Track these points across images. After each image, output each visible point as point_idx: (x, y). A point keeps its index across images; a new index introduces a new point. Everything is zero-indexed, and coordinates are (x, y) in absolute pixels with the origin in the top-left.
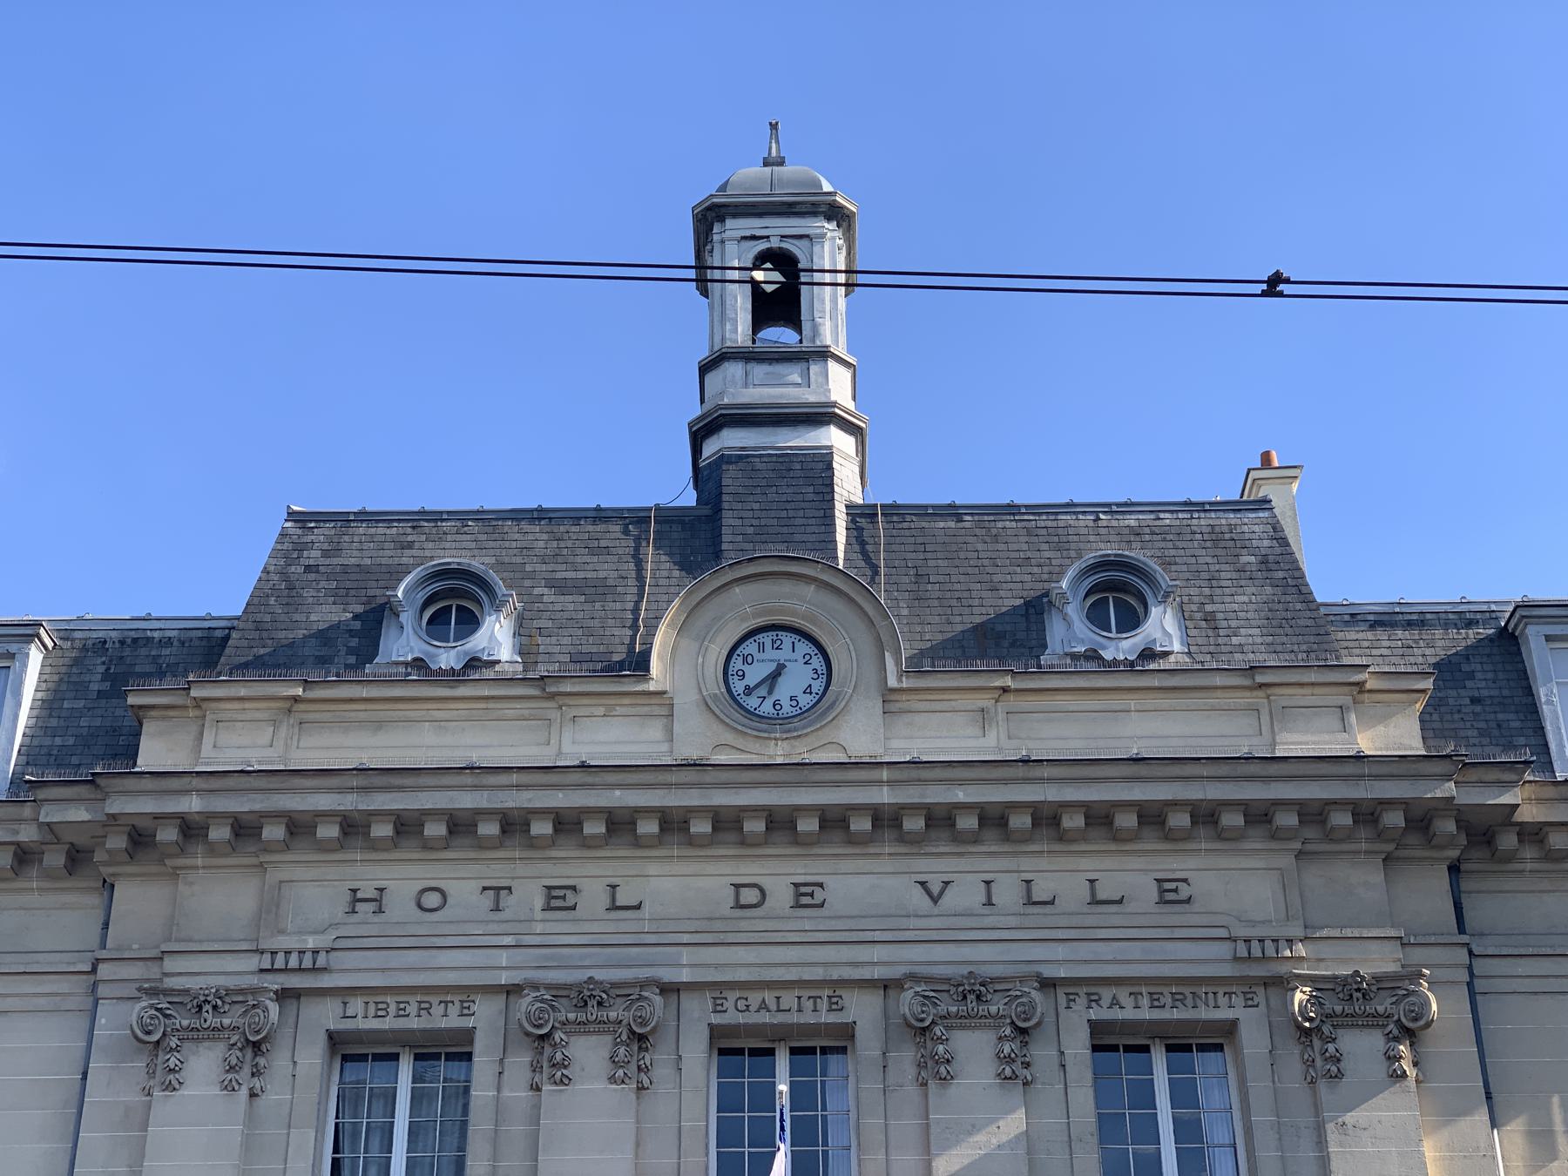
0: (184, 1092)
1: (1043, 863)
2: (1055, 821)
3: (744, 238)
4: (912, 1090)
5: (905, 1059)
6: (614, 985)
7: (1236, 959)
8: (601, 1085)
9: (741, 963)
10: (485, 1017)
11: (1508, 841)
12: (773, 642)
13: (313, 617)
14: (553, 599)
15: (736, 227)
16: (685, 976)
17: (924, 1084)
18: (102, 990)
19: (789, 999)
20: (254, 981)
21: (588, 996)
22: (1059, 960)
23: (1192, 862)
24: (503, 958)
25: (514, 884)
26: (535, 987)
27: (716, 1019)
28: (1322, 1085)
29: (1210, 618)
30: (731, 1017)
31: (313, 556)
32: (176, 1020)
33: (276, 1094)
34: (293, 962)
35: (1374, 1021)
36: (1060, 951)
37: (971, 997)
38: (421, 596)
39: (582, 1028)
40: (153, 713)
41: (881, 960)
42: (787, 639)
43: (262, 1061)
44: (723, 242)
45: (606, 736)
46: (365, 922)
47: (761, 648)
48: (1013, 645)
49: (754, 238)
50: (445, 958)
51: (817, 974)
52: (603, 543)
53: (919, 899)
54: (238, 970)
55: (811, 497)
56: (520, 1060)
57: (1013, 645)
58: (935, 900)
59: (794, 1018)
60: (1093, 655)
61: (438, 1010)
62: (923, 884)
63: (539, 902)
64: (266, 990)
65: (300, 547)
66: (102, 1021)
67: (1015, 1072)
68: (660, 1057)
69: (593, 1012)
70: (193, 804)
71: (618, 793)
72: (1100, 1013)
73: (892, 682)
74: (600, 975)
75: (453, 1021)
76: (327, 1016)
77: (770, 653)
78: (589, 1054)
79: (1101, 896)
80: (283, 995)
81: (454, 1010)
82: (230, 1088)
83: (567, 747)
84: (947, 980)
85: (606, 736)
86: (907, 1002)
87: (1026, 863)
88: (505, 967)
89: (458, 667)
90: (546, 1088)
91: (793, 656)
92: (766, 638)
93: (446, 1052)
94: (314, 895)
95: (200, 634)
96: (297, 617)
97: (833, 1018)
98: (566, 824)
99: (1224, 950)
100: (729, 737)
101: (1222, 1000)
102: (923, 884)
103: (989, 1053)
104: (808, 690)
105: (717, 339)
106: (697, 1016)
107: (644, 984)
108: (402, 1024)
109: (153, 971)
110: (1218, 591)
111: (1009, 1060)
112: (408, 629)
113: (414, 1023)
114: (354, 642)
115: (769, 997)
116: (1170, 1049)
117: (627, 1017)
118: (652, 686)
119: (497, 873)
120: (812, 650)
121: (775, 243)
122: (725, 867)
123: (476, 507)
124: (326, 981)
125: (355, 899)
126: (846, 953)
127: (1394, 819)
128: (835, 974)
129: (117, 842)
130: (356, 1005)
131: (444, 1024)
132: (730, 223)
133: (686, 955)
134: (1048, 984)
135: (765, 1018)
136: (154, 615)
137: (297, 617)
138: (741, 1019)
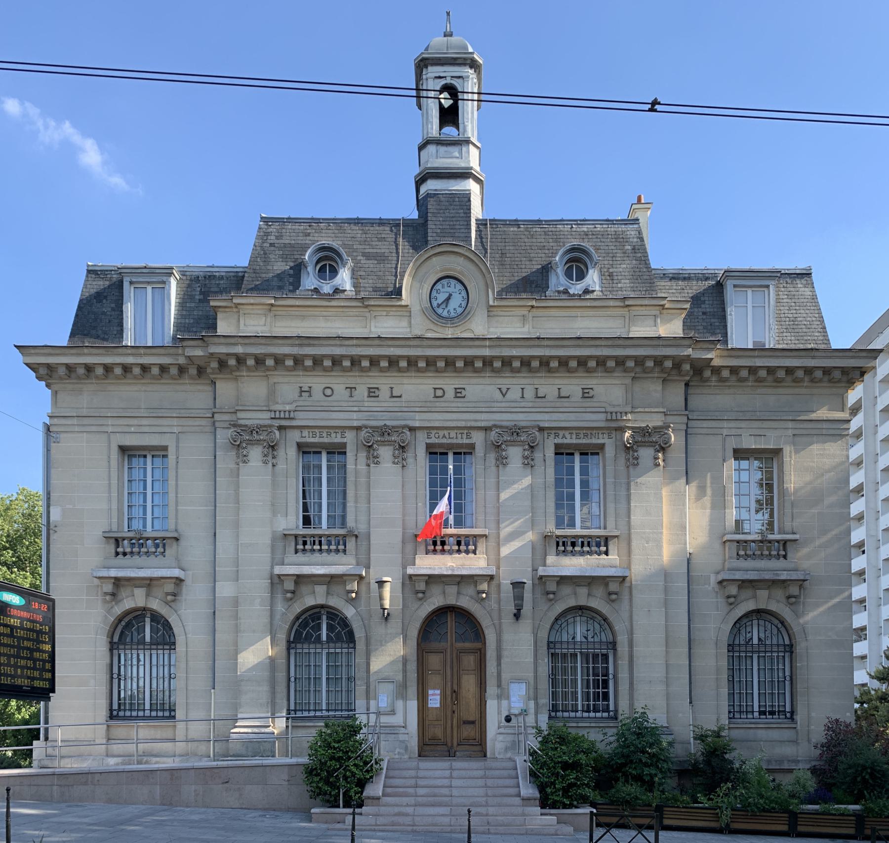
1: (542, 381)
3: (436, 77)
4: (494, 469)
5: (492, 457)
6: (393, 427)
7: (607, 420)
8: (390, 465)
9: (436, 419)
11: (707, 373)
16: (417, 424)
18: (217, 424)
21: (384, 431)
22: (546, 420)
25: (357, 386)
27: (428, 441)
29: (611, 275)
30: (434, 440)
32: (244, 438)
33: (281, 466)
35: (652, 444)
38: (315, 259)
39: (383, 443)
41: (485, 420)
42: (453, 282)
43: (275, 453)
46: (305, 401)
47: (443, 287)
48: (536, 286)
49: (440, 77)
51: (463, 424)
52: (383, 236)
53: (498, 396)
54: (262, 418)
55: (462, 215)
56: (363, 455)
57: (536, 286)
60: (566, 292)
61: (333, 435)
63: (366, 394)
65: (267, 234)
66: (218, 436)
68: (409, 455)
69: (387, 438)
72: (559, 441)
73: (491, 303)
76: (295, 436)
78: (385, 453)
79: (562, 395)
80: (280, 428)
81: (339, 435)
82: (265, 462)
83: (373, 329)
86: (493, 435)
87: (536, 381)
92: (445, 282)
93: (337, 451)
99: (602, 416)
100: (432, 326)
103: (520, 455)
104: (460, 306)
106: (422, 440)
107: (404, 427)
108: (321, 440)
109: (234, 417)
111: (526, 458)
113: (326, 440)
115: (446, 432)
117: (398, 439)
118: (403, 303)
120: (462, 287)
121: (448, 81)
122: (430, 381)
123: (333, 217)
124: (294, 423)
127: (668, 364)
129: (214, 365)
130: (305, 433)
131: (336, 441)
132: (430, 68)
134: (541, 429)
135: (444, 441)
136: (216, 265)
138: (437, 441)
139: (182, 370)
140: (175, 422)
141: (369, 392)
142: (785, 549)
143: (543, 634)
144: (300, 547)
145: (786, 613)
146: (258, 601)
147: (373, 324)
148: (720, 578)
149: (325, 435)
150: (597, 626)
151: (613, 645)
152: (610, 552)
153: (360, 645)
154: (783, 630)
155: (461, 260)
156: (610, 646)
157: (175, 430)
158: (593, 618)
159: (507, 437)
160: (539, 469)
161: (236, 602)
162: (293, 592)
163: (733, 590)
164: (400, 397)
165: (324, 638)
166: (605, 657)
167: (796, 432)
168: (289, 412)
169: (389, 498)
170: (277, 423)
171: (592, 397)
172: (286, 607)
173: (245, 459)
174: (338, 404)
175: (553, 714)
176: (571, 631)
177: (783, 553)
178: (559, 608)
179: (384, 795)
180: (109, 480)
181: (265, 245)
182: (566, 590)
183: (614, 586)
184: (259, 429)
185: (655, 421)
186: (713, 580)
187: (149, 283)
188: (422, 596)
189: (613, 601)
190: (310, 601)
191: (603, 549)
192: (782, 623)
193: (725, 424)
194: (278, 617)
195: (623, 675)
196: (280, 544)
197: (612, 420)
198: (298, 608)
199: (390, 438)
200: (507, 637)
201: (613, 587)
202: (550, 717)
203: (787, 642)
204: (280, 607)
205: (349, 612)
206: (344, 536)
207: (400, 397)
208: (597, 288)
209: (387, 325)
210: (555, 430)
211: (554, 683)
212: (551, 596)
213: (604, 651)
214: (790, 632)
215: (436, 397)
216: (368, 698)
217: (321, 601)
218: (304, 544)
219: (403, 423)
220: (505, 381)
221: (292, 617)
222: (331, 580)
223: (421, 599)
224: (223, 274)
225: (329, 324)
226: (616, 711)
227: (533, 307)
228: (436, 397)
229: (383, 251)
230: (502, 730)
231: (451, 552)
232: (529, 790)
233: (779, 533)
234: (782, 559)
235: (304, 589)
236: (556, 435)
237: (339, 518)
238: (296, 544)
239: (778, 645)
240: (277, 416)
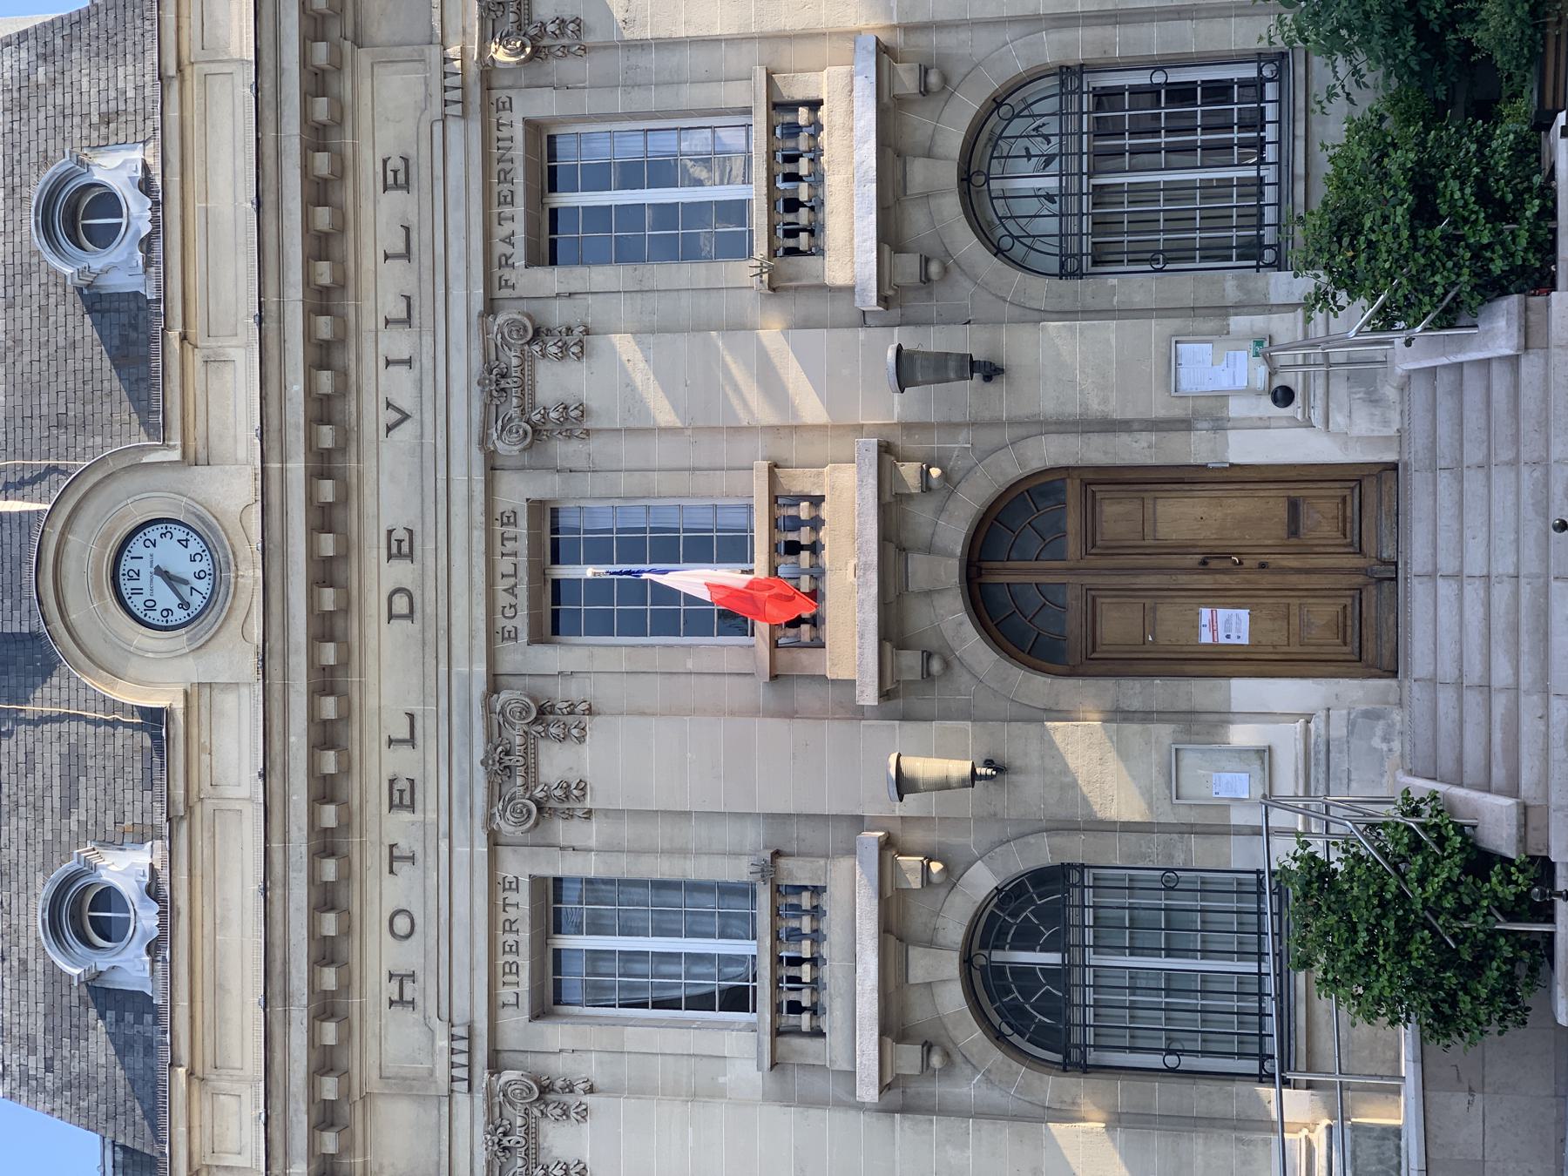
2: (324, 292)
4: (594, 444)
5: (564, 450)
6: (489, 739)
7: (464, 115)
8: (586, 750)
9: (468, 614)
12: (131, 579)
14: (82, 810)
16: (481, 669)
19: (505, 565)
20: (479, 1097)
21: (500, 766)
22: (466, 295)
24: (461, 850)
25: (387, 842)
26: (490, 818)
27: (524, 637)
28: (588, 424)
30: (522, 623)
31: (35, 1064)
33: (590, 1068)
34: (462, 1059)
36: (458, 292)
37: (503, 383)
38: (80, 949)
39: (531, 770)
42: (127, 564)
43: (559, 1083)
45: (232, 751)
46: (424, 991)
47: (137, 591)
48: (135, 328)
50: (461, 909)
51: (479, 536)
52: (22, 758)
53: (406, 432)
54: (469, 1113)
56: (563, 831)
58: (405, 417)
59: (523, 560)
60: (146, 244)
61: (512, 913)
62: (389, 429)
63: (405, 816)
64: (489, 1084)
67: (576, 342)
69: (516, 760)
70: (297, 467)
71: (292, 739)
72: (519, 256)
73: (176, 455)
74: (479, 754)
75: (523, 898)
76: (516, 1024)
77: (143, 582)
80: (495, 1066)
81: (512, 897)
82: (584, 1114)
84: (486, 406)
85: (232, 751)
86: (508, 448)
87: (368, 323)
88: (471, 848)
90: (588, 804)
91: (147, 559)
92: (127, 586)
94: (395, 1042)
96: (102, 1078)
98: (325, 790)
99: (455, 128)
101: (505, 132)
102: (389, 429)
104: (184, 543)
106: (520, 656)
108: (525, 949)
110: (77, 108)
111: (564, 348)
112: (115, 961)
113: (525, 936)
114: (129, 1017)
115: (501, 585)
116: (553, 188)
117: (520, 726)
118: (179, 705)
119: (375, 859)
124: (482, 1026)
125: (400, 1001)
126: (459, 508)
128: (479, 518)
130: (507, 994)
131: (525, 906)
133: (460, 668)
135: (523, 590)
137: (102, 1078)
138: (523, 612)
143: (1040, 290)
146: (951, 1153)
147: (230, 792)
149: (510, 938)
150: (1017, 127)
151: (1069, 75)
152: (811, 94)
153: (1075, 849)
156: (1073, 84)
158: (995, 140)
159: (514, 412)
160: (594, 310)
162: (928, 1047)
165: (1054, 958)
166: (1104, 97)
172: (968, 1070)
173: (574, 791)
174: (434, 898)
175: (1269, 256)
176: (1032, 206)
178: (966, 243)
179: (1513, 791)
182: (917, 222)
183: (907, 83)
184: (498, 1130)
189: (945, 80)
190: (953, 998)
191: (803, 115)
194: (995, 1097)
196: (799, 1080)
198: (971, 1035)
200: (1048, 404)
201: (907, 80)
202: (1279, 265)
204: (968, 1089)
205: (982, 881)
206: (777, 890)
208: (137, 155)
210: (492, 264)
211: (1176, 255)
212: (934, 268)
213: (1087, 102)
215: (410, 615)
216: (1226, 831)
217: (951, 966)
218: (797, 1012)
221: (996, 1056)
222: (895, 932)
223: (947, 665)
225: (235, 915)
226: (1260, 58)
227: (184, 338)
228: (410, 615)
229: (56, 759)
230: (1317, 416)
232: (1498, 332)
234: (823, 112)
235: (919, 1014)
237: (723, 904)
238: (797, 1032)
240: (463, 1045)
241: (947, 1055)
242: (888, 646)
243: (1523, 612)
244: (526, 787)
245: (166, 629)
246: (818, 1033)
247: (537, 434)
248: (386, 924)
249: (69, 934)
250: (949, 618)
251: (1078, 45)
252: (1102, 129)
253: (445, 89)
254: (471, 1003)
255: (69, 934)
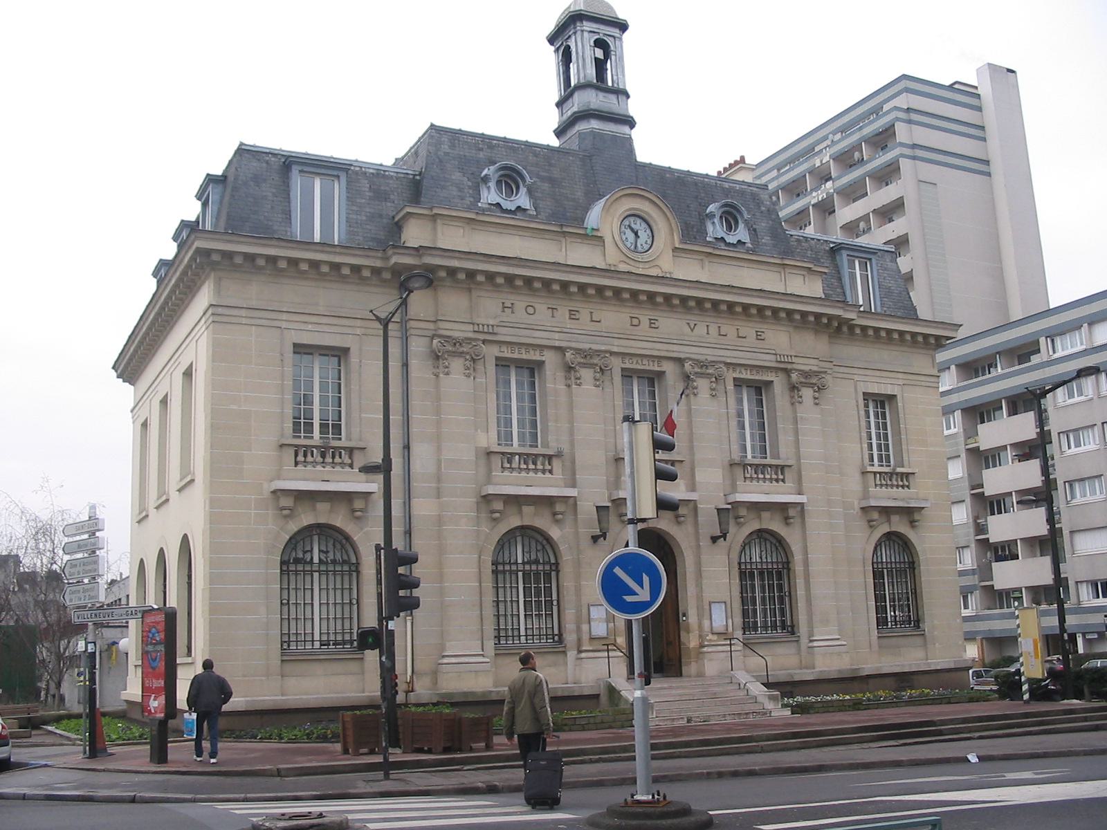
0: (582, 387)
1: (724, 321)
3: (591, 32)
6: (597, 351)
7: (777, 361)
10: (549, 358)
13: (454, 177)
15: (588, 26)
17: (569, 386)
20: (471, 335)
21: (586, 354)
23: (766, 326)
24: (557, 336)
25: (558, 307)
27: (624, 366)
29: (755, 230)
30: (628, 365)
35: (811, 385)
37: (458, 344)
39: (584, 365)
40: (414, 216)
43: (800, 393)
44: (582, 31)
46: (507, 317)
48: (697, 232)
49: (594, 32)
50: (538, 334)
58: (692, 330)
62: (688, 324)
63: (567, 316)
64: (479, 339)
67: (597, 383)
68: (480, 366)
69: (703, 370)
70: (455, 263)
72: (737, 375)
73: (677, 246)
76: (492, 352)
78: (587, 374)
79: (740, 335)
84: (697, 360)
87: (720, 321)
89: (513, 209)
93: (532, 369)
95: (402, 175)
97: (659, 369)
99: (773, 358)
100: (624, 259)
101: (651, 363)
102: (688, 324)
105: (582, 75)
107: (606, 352)
116: (516, 367)
117: (600, 363)
120: (647, 227)
121: (601, 36)
122: (628, 310)
131: (534, 358)
132: (585, 23)
133: (616, 342)
139: (376, 271)
140: (900, 376)
141: (570, 314)
142: (350, 457)
144: (300, 458)
145: (349, 528)
148: (864, 504)
151: (787, 565)
152: (555, 471)
154: (548, 547)
155: (647, 203)
157: (358, 331)
158: (530, 537)
159: (697, 370)
161: (440, 521)
163: (498, 505)
164: (599, 322)
167: (905, 382)
168: (493, 326)
169: (712, 426)
170: (482, 337)
171: (578, 319)
174: (541, 323)
177: (550, 467)
180: (859, 422)
181: (439, 153)
185: (811, 365)
186: (857, 506)
187: (857, 257)
188: (290, 514)
192: (906, 543)
193: (855, 371)
195: (800, 592)
197: (781, 362)
199: (461, 349)
200: (705, 558)
203: (553, 561)
204: (485, 529)
207: (599, 322)
209: (580, 255)
214: (556, 551)
219: (603, 348)
220: (510, 299)
223: (286, 517)
224: (392, 174)
231: (315, 463)
233: (773, 457)
234: (781, 483)
236: (734, 371)
238: (296, 455)
239: (772, 563)
240: (481, 329)
241: (286, 517)
242: (295, 493)
243: (159, 769)
244: (579, 363)
245: (653, 237)
246: (296, 464)
247: (436, 357)
248: (531, 304)
249: (502, 172)
250: (306, 519)
251: (798, 567)
252: (770, 573)
253: (488, 326)
254: (505, 334)
255: (502, 172)
